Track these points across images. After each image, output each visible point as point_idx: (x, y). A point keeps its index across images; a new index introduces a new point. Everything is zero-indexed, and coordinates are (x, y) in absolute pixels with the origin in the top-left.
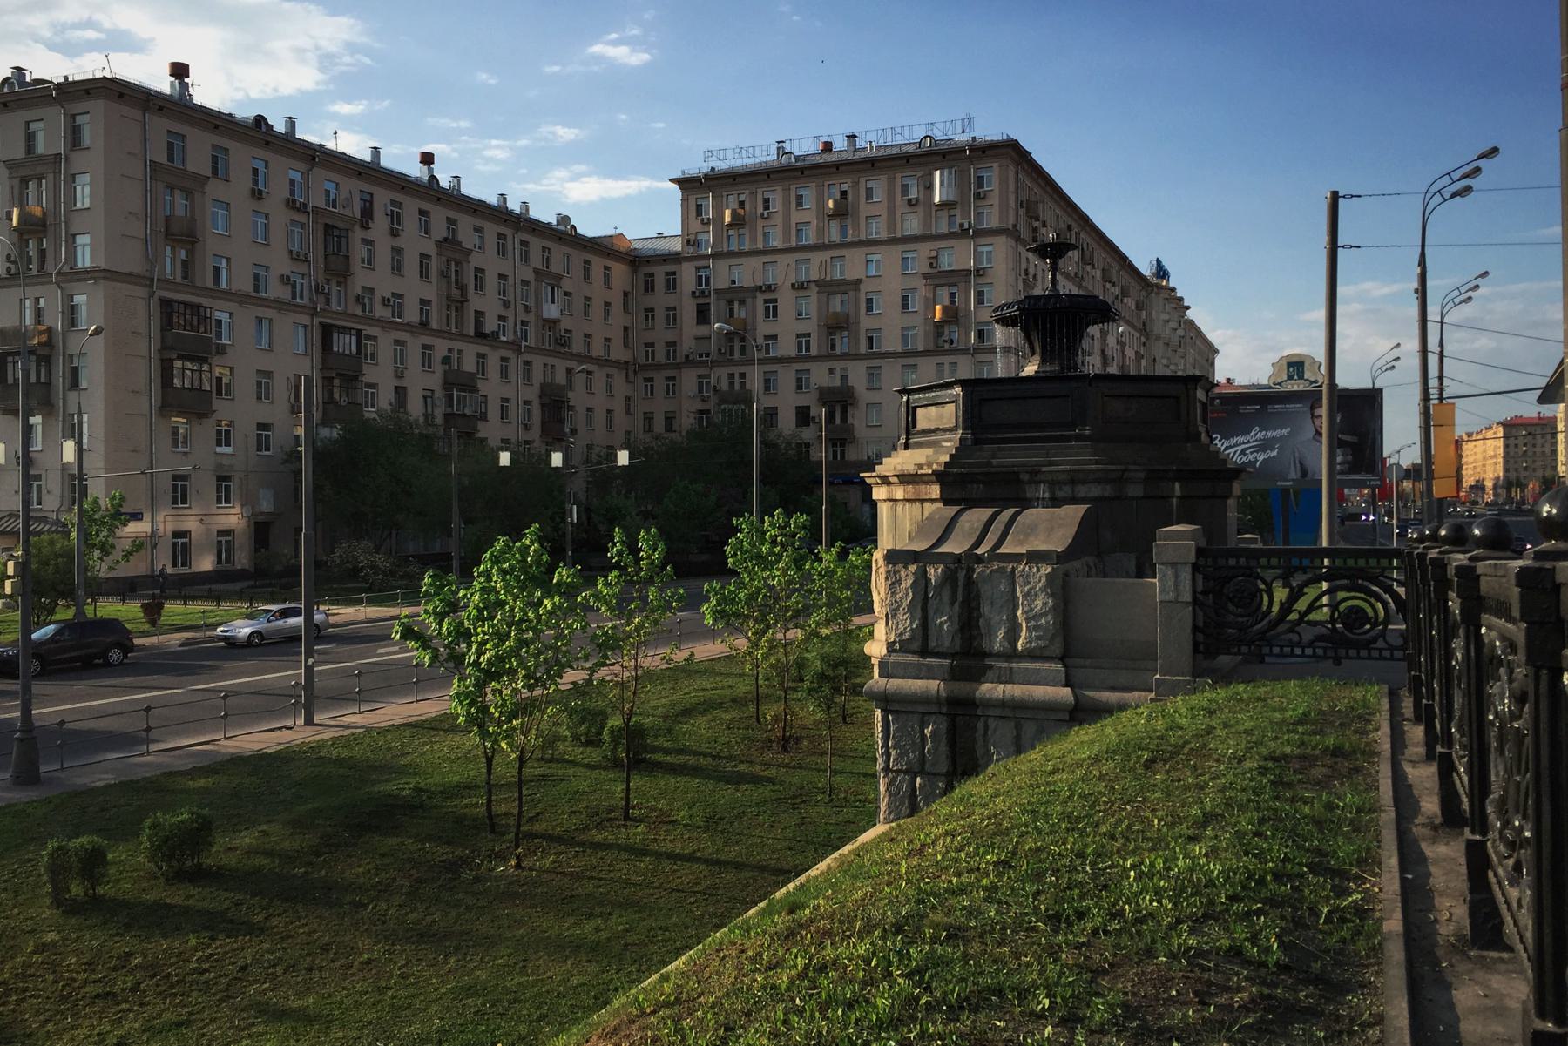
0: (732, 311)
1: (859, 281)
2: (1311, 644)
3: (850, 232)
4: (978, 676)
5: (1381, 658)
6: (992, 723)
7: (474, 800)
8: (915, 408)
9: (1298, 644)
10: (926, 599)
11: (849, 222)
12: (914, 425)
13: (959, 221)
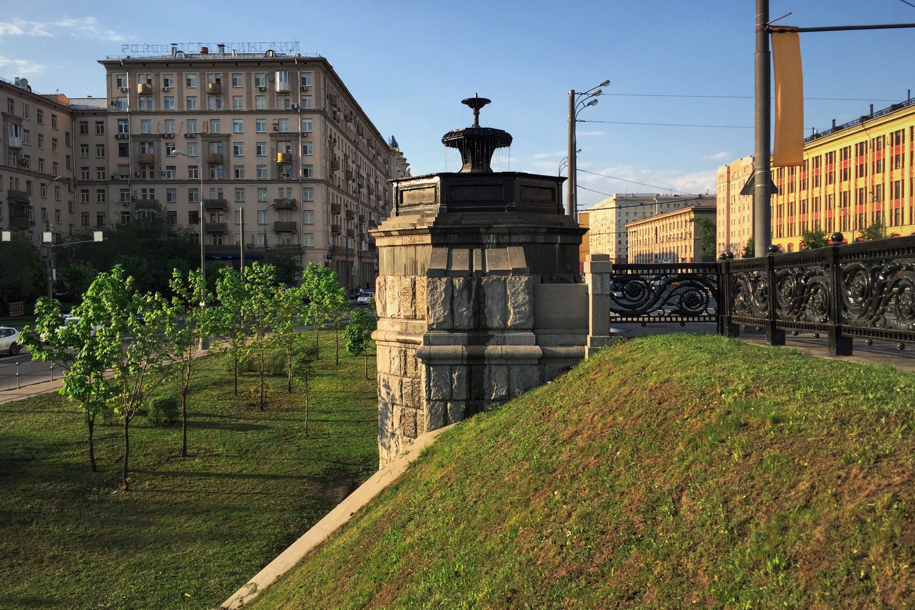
0: (144, 149)
1: (229, 136)
2: (669, 316)
3: (223, 104)
4: (485, 341)
5: (705, 321)
6: (494, 369)
7: (71, 452)
8: (402, 192)
9: (663, 316)
10: (452, 297)
11: (222, 98)
12: (402, 202)
13: (291, 103)
